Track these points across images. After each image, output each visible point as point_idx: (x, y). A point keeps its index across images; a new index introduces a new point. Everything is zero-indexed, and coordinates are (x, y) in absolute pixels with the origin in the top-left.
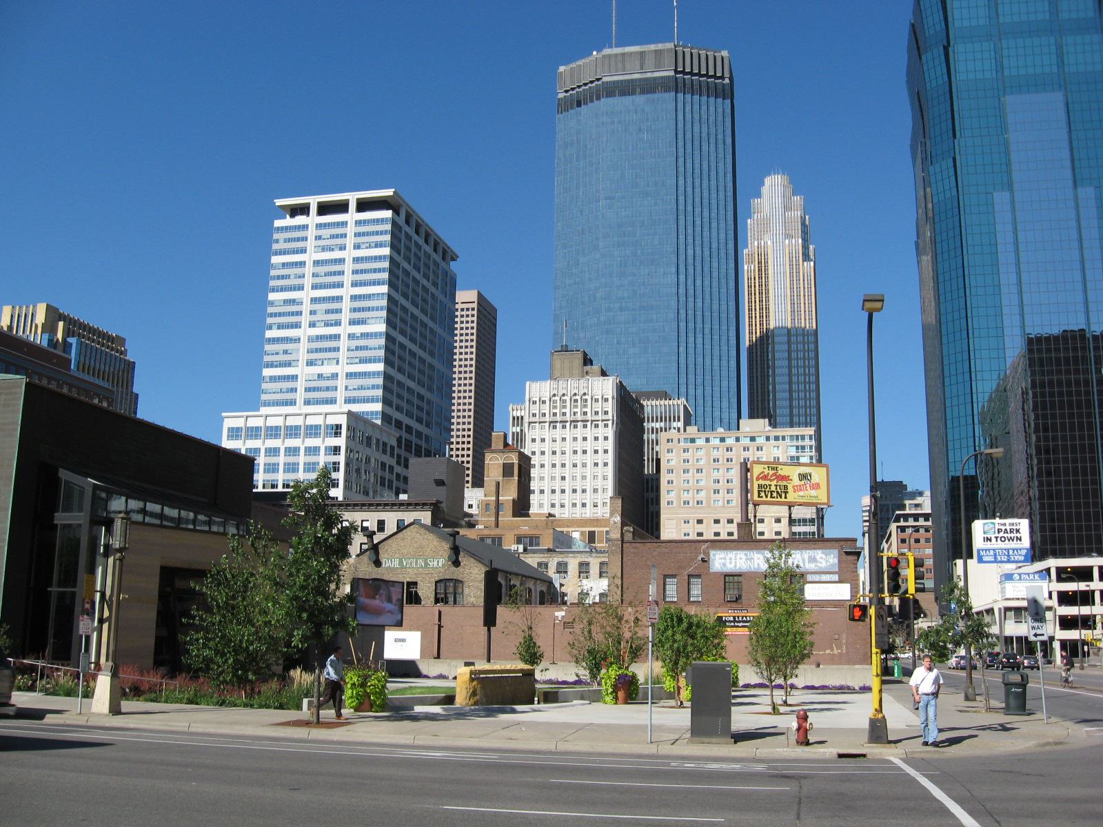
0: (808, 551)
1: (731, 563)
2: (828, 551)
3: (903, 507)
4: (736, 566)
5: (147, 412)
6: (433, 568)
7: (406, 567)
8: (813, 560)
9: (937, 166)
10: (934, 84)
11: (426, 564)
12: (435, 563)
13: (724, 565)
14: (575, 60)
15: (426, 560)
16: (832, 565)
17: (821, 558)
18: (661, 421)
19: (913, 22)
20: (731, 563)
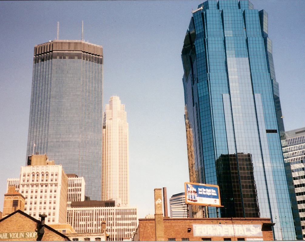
0: (245, 225)
1: (204, 231)
2: (256, 225)
3: (125, 111)
4: (207, 233)
5: (304, 126)
6: (29, 238)
7: (12, 238)
8: (249, 230)
9: (201, 84)
10: (199, 52)
11: (25, 236)
12: (31, 235)
13: (201, 232)
14: (94, 44)
15: (25, 233)
16: (259, 233)
17: (253, 229)
18: (80, 225)
19: (189, 30)
20: (204, 231)
